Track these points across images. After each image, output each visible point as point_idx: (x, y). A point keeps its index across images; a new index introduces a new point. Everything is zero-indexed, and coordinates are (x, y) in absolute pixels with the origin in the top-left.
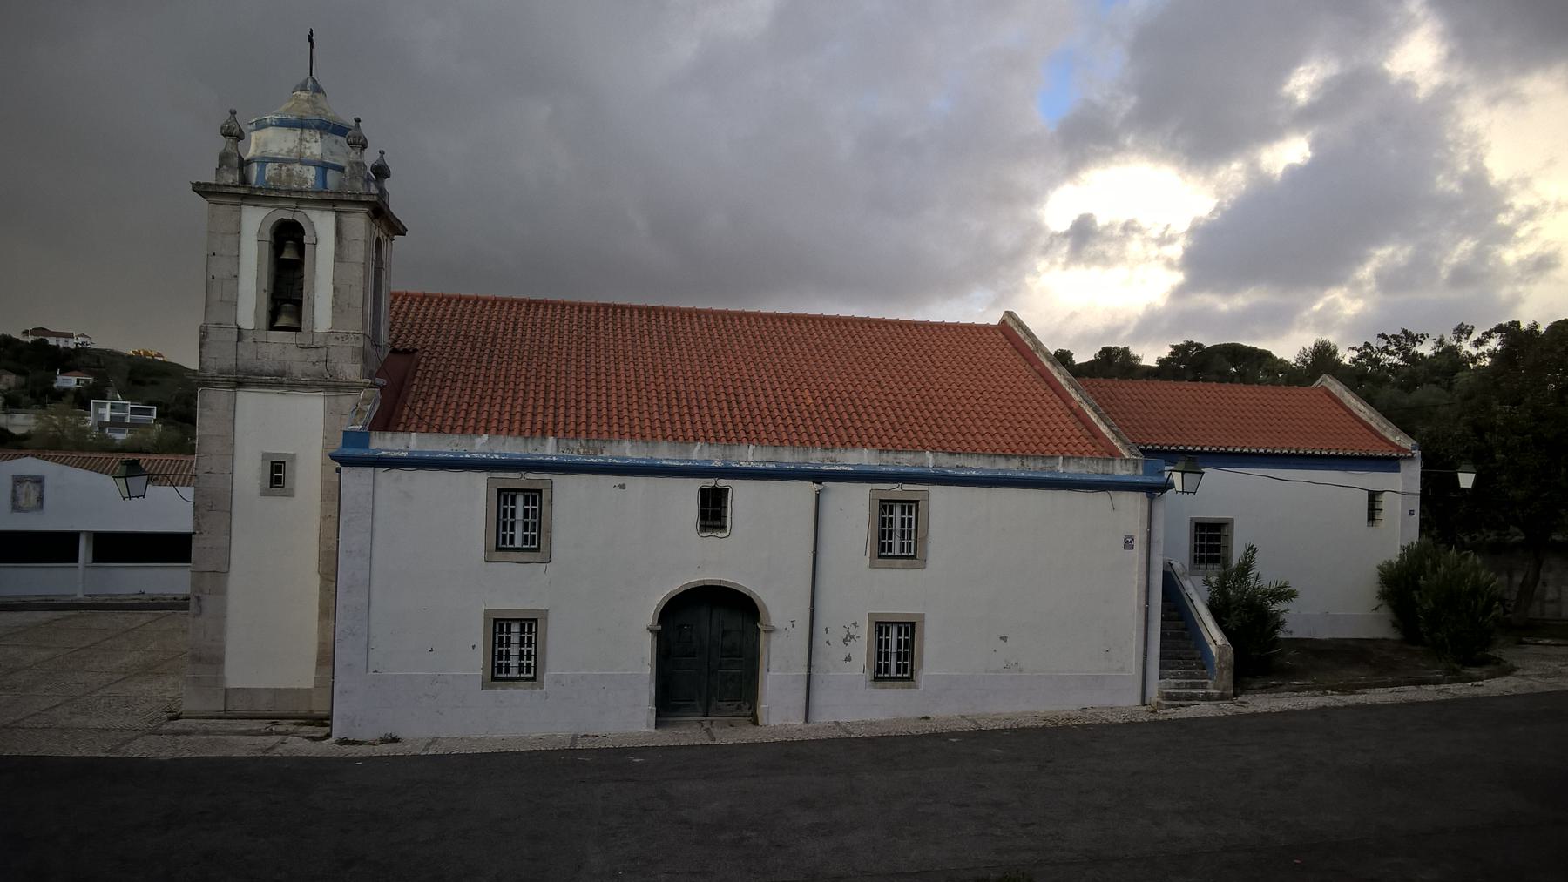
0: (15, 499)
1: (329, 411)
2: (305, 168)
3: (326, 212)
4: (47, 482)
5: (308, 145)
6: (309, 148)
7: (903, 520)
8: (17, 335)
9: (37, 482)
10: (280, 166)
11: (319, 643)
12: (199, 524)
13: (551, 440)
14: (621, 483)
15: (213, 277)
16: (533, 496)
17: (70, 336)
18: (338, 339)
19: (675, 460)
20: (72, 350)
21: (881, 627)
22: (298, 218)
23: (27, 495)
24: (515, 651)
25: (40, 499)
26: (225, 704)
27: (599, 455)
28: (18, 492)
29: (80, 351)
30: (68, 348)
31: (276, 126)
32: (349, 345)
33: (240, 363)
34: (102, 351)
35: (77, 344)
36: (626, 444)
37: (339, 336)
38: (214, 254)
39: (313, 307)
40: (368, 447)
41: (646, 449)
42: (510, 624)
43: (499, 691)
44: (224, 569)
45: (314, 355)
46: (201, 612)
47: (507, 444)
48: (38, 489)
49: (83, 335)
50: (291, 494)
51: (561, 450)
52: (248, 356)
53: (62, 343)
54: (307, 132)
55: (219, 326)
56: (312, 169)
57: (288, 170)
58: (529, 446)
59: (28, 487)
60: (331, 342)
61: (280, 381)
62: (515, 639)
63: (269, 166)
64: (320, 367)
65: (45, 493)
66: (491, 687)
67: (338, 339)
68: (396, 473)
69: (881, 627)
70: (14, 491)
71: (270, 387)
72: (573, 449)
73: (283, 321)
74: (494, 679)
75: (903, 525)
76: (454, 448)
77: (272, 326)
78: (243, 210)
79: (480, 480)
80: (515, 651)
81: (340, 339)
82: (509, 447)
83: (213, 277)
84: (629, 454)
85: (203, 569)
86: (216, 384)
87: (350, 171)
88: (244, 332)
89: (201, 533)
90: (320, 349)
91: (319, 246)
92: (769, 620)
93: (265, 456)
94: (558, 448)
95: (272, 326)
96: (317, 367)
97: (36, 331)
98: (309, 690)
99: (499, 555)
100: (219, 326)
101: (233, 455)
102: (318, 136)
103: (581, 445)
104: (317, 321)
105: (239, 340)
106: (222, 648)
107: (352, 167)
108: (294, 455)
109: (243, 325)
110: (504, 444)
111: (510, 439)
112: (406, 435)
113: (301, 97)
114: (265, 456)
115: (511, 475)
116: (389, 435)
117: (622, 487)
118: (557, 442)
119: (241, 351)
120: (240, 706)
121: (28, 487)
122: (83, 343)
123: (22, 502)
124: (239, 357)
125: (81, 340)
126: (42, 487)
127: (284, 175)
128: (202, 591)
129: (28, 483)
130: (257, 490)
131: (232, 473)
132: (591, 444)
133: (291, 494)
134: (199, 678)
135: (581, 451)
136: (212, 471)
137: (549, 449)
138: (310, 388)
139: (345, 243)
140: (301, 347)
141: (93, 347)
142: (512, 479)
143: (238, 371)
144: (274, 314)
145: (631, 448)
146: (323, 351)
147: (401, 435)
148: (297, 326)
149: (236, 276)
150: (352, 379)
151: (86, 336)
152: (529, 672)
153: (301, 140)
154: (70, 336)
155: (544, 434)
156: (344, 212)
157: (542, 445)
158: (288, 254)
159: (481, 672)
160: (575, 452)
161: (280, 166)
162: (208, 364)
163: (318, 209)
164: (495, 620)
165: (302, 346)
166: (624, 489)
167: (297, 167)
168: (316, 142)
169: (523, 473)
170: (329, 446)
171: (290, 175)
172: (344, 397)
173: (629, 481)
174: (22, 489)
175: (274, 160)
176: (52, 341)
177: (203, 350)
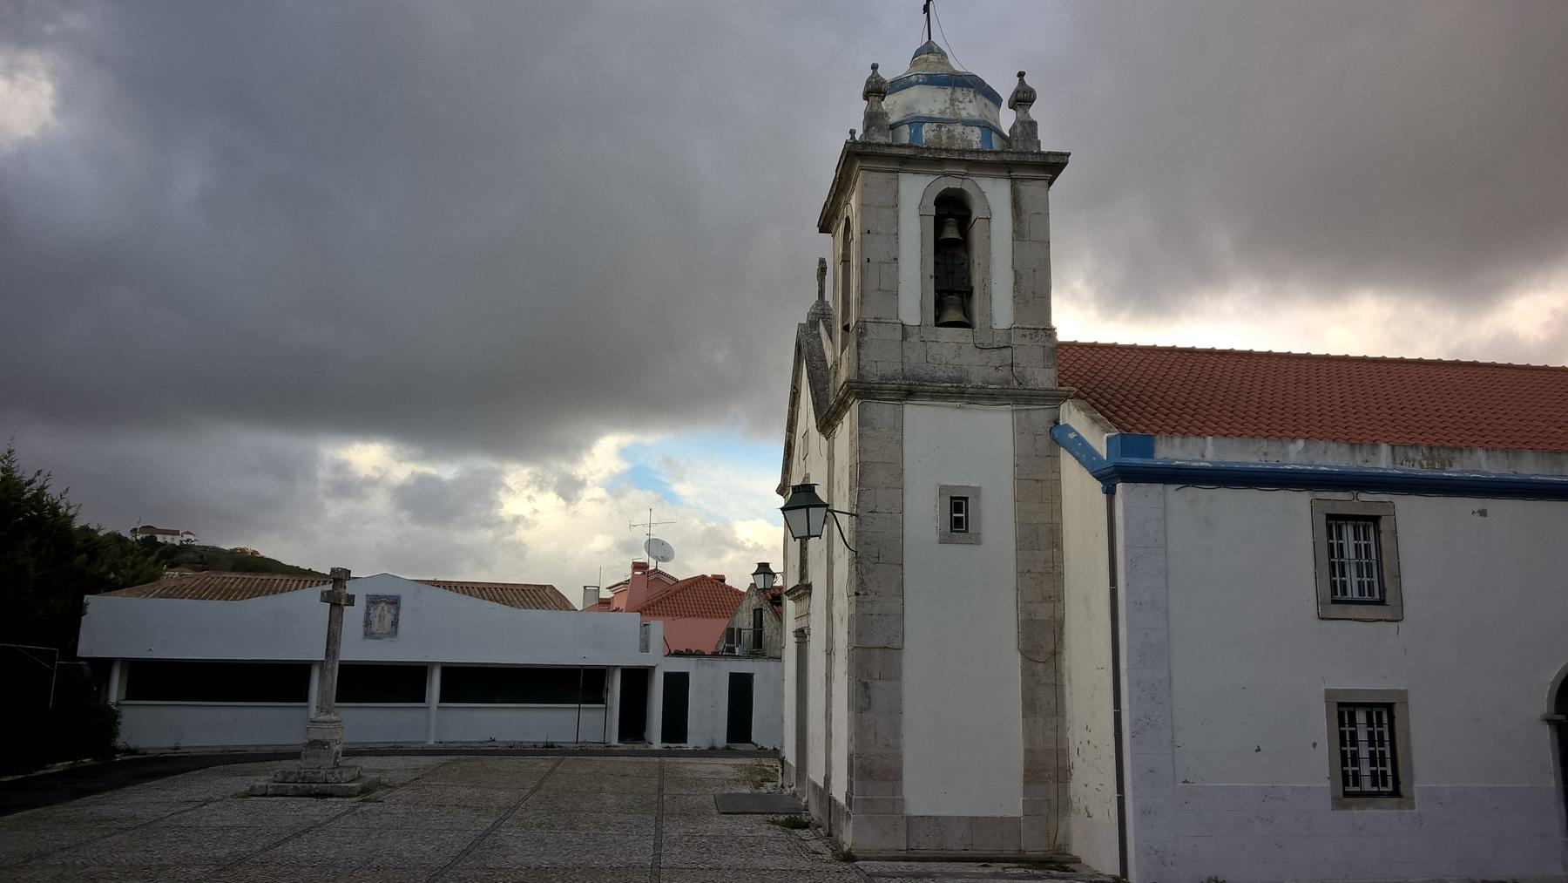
0: (368, 623)
1: (1019, 430)
2: (968, 129)
3: (998, 180)
4: (403, 603)
5: (961, 106)
6: (964, 109)
7: (1357, 547)
8: (126, 534)
9: (392, 603)
10: (939, 127)
11: (1025, 750)
12: (863, 582)
13: (1385, 449)
14: (1482, 508)
15: (869, 261)
16: (1369, 522)
17: (176, 533)
18: (1025, 336)
19: (1541, 476)
20: (178, 547)
21: (1345, 710)
22: (966, 186)
23: (381, 618)
24: (1364, 752)
25: (395, 623)
26: (907, 841)
27: (1447, 468)
28: (372, 615)
29: (185, 548)
30: (174, 545)
31: (923, 84)
32: (1040, 343)
33: (906, 369)
34: (205, 548)
35: (181, 541)
36: (1481, 454)
37: (1027, 332)
38: (869, 232)
39: (990, 297)
40: (1152, 457)
41: (1506, 461)
42: (1354, 712)
43: (1355, 812)
44: (897, 644)
45: (996, 358)
46: (870, 704)
47: (1329, 453)
48: (393, 611)
49: (188, 533)
50: (976, 541)
51: (1398, 461)
52: (916, 360)
53: (169, 539)
54: (959, 91)
55: (878, 321)
56: (977, 131)
57: (949, 131)
58: (1358, 456)
59: (383, 610)
60: (1016, 340)
61: (959, 392)
62: (1362, 736)
63: (926, 127)
64: (1005, 372)
65: (400, 617)
66: (1346, 807)
67: (1025, 336)
68: (1191, 492)
69: (1345, 710)
70: (368, 614)
71: (945, 398)
72: (1414, 460)
73: (953, 315)
74: (1396, 793)
75: (1358, 555)
76: (1263, 458)
77: (939, 322)
78: (900, 177)
79: (1300, 502)
80: (1364, 752)
81: (1029, 337)
82: (1332, 458)
83: (869, 261)
84: (1485, 468)
85: (869, 645)
86: (881, 394)
87: (1022, 132)
88: (908, 329)
89: (866, 594)
90: (1004, 350)
91: (992, 221)
92: (903, 808)
93: (943, 489)
94: (1394, 459)
95: (939, 322)
96: (1000, 373)
97: (145, 529)
98: (1015, 820)
99: (1336, 610)
100: (878, 321)
101: (902, 489)
102: (972, 95)
103: (1423, 454)
104: (996, 315)
105: (904, 338)
106: (899, 758)
107: (1024, 128)
108: (978, 489)
109: (906, 321)
110: (1325, 453)
111: (1333, 446)
112: (1199, 440)
113: (931, 60)
114: (943, 489)
115: (1340, 496)
116: (1177, 440)
117: (1483, 513)
118: (1393, 450)
119: (907, 353)
120: (928, 844)
121: (383, 610)
122: (188, 540)
123: (375, 627)
124: (905, 360)
125: (186, 537)
126: (398, 609)
127: (944, 137)
128: (869, 675)
129: (383, 604)
130: (935, 537)
131: (902, 512)
132: (1435, 453)
133: (976, 541)
134: (871, 800)
135: (1424, 463)
136: (877, 510)
137: (1383, 461)
138: (996, 399)
139: (1025, 217)
140: (980, 348)
141: (196, 543)
142: (1342, 501)
143: (904, 378)
144: (940, 306)
145: (1488, 459)
146: (1007, 352)
147: (1193, 440)
148: (965, 320)
149: (896, 259)
150: (1046, 386)
151: (191, 534)
152: (1385, 784)
153: (952, 100)
154: (176, 533)
155: (1375, 444)
156: (1022, 179)
157: (1373, 455)
158: (951, 233)
159: (1327, 784)
160: (1416, 465)
161: (939, 127)
162: (868, 368)
163: (990, 176)
164: (1340, 705)
165: (981, 346)
166: (1486, 516)
167: (959, 129)
168: (970, 102)
169: (1355, 493)
170: (1022, 477)
171: (951, 137)
172: (1037, 412)
173: (1491, 505)
174: (376, 612)
175: (931, 120)
176: (160, 538)
177: (861, 351)
